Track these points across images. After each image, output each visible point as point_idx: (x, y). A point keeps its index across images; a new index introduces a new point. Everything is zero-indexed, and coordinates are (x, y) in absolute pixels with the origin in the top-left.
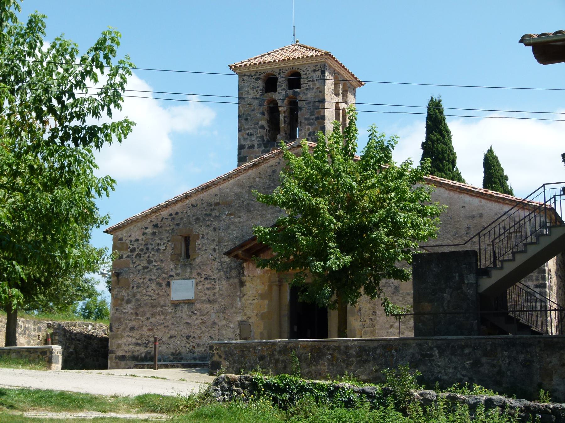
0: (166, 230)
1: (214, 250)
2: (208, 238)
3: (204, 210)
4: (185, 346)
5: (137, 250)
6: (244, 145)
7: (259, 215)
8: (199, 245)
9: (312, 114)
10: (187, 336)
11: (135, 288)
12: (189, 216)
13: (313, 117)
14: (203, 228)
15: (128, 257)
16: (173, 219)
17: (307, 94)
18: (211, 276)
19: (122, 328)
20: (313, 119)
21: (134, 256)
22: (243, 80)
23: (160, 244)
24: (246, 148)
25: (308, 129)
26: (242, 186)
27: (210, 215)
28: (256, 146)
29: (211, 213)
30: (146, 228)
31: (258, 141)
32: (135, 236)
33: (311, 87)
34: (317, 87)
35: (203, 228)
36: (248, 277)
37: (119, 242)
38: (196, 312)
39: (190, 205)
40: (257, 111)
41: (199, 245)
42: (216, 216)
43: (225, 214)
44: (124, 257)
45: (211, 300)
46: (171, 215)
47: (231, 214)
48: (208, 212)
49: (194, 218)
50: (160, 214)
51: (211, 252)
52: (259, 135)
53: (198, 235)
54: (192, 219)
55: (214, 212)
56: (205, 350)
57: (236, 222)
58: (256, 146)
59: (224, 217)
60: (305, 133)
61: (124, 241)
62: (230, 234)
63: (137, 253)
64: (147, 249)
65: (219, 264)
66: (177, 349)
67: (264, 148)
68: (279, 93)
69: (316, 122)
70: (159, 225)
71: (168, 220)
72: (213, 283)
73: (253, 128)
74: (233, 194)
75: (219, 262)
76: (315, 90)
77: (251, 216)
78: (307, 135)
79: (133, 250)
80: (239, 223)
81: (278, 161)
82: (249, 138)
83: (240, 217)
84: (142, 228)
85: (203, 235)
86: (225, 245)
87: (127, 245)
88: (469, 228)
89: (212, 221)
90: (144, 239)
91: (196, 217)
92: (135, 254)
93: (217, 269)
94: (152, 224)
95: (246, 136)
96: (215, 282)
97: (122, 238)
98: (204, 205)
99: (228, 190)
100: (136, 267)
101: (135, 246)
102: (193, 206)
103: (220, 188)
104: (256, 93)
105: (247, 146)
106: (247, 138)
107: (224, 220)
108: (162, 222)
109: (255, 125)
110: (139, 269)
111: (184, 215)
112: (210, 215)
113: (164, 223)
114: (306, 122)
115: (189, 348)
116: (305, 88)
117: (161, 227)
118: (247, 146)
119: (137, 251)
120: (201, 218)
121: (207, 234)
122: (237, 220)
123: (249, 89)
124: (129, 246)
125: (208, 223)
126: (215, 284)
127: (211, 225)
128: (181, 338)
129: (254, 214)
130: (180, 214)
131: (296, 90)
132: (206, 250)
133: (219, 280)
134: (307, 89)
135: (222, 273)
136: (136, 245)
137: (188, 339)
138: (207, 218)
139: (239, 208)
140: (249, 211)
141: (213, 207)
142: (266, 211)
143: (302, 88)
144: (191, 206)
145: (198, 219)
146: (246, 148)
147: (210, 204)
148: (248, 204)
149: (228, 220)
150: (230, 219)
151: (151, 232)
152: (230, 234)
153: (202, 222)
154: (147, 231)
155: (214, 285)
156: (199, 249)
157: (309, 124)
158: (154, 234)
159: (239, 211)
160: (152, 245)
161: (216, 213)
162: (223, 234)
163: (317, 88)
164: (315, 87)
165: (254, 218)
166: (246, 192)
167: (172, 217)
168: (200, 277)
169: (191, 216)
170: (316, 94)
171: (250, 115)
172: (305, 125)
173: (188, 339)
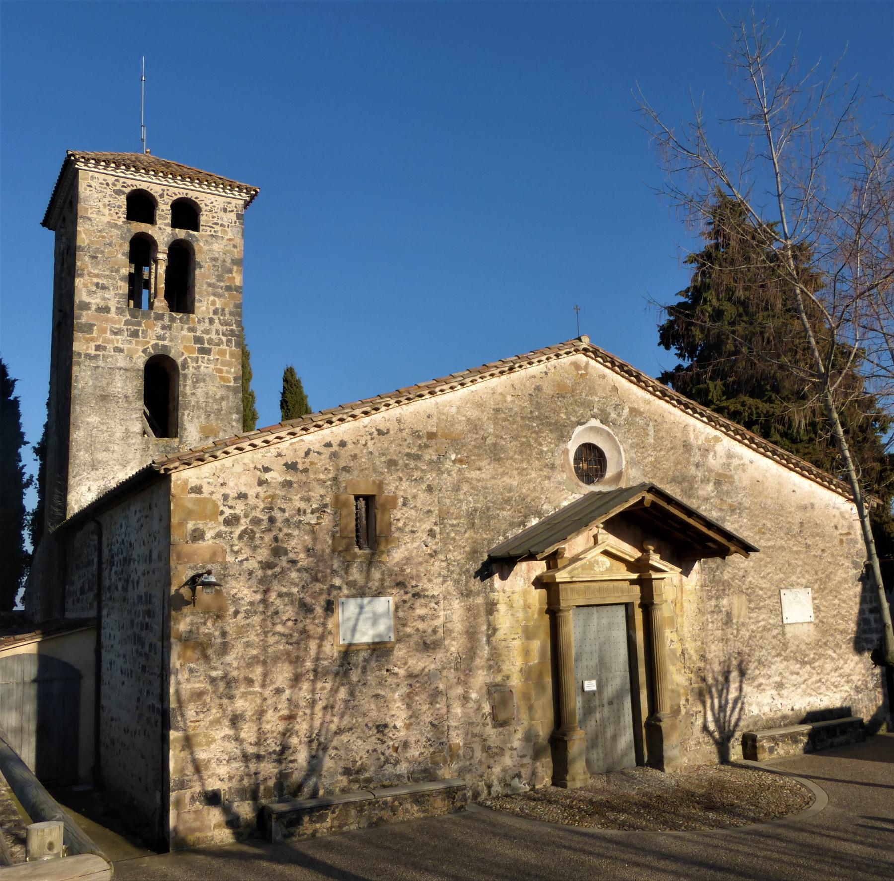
0: (319, 480)
1: (431, 533)
2: (415, 507)
3: (406, 443)
4: (375, 750)
5: (243, 521)
6: (90, 303)
7: (517, 469)
8: (398, 520)
9: (220, 278)
10: (378, 727)
11: (240, 616)
12: (371, 453)
13: (222, 284)
14: (405, 485)
15: (219, 535)
16: (334, 455)
17: (211, 243)
18: (426, 590)
19: (208, 719)
20: (221, 288)
21: (236, 535)
22: (90, 186)
23: (305, 512)
24: (93, 309)
25: (213, 303)
26: (480, 406)
27: (418, 457)
28: (113, 309)
29: (420, 453)
30: (266, 469)
31: (118, 302)
32: (236, 485)
33: (219, 234)
34: (229, 237)
35: (405, 485)
36: (501, 594)
37: (193, 495)
38: (396, 670)
39: (374, 430)
40: (118, 248)
41: (398, 520)
42: (431, 462)
43: (450, 459)
44: (208, 535)
45: (428, 642)
46: (328, 445)
47: (461, 461)
48: (414, 450)
49: (383, 459)
50: (302, 440)
51: (424, 538)
52: (121, 292)
53: (395, 498)
54: (380, 462)
55: (426, 451)
56: (422, 754)
57: (472, 478)
58: (113, 309)
59: (448, 464)
60: (207, 308)
61: (205, 495)
62: (461, 501)
63: (243, 528)
64: (272, 520)
65: (444, 564)
66: (357, 759)
67: (129, 317)
68: (160, 228)
69: (227, 294)
70: (300, 467)
71: (323, 456)
72: (433, 605)
73: (107, 277)
74: (464, 419)
75: (443, 561)
76: (225, 242)
77: (500, 470)
78: (211, 311)
79: (232, 521)
80: (479, 480)
81: (545, 369)
82: (100, 293)
83: (480, 469)
84: (255, 468)
85: (405, 499)
86: (453, 525)
87: (216, 506)
88: (801, 524)
89: (422, 470)
90: (262, 495)
91: (389, 457)
92: (238, 531)
93: (439, 574)
94: (282, 461)
95: (94, 288)
96: (436, 603)
97: (201, 487)
98: (404, 434)
99: (454, 410)
100: (241, 562)
101: (238, 511)
102: (380, 433)
103: (437, 404)
104: (115, 217)
105: (94, 307)
106: (95, 292)
107: (449, 472)
108: (307, 460)
109: (112, 272)
110: (251, 568)
111: (361, 451)
112: (418, 457)
113: (312, 463)
114: (210, 289)
115: (383, 754)
116: (208, 233)
117: (306, 470)
118: (94, 307)
119: (244, 524)
120: (401, 462)
121: (414, 497)
122: (475, 474)
123: (101, 204)
124: (222, 508)
125: (417, 474)
126: (436, 607)
127: (421, 478)
128: (364, 732)
129: (507, 465)
130: (350, 446)
131: (191, 232)
132: (413, 532)
133: (445, 598)
134: (212, 235)
135: (450, 583)
136: (240, 508)
137: (382, 732)
138: (412, 464)
139: (476, 451)
140: (498, 460)
141: (425, 440)
142: (529, 462)
143: (201, 232)
144: (376, 433)
145: (392, 463)
146: (93, 309)
147: (416, 434)
148: (495, 445)
149: (457, 473)
150: (460, 470)
151: (280, 479)
152: (461, 501)
153: (403, 470)
154: (268, 476)
155: (435, 610)
156: (399, 529)
157: (214, 295)
158: (287, 484)
159: (479, 455)
160: (283, 511)
161: (431, 455)
162: (448, 501)
163: (230, 240)
164: (226, 237)
165: (507, 473)
166: (488, 419)
167: (332, 449)
168: (402, 592)
169: (376, 453)
170: (227, 248)
171: (102, 253)
172: (208, 294)
173: (382, 732)
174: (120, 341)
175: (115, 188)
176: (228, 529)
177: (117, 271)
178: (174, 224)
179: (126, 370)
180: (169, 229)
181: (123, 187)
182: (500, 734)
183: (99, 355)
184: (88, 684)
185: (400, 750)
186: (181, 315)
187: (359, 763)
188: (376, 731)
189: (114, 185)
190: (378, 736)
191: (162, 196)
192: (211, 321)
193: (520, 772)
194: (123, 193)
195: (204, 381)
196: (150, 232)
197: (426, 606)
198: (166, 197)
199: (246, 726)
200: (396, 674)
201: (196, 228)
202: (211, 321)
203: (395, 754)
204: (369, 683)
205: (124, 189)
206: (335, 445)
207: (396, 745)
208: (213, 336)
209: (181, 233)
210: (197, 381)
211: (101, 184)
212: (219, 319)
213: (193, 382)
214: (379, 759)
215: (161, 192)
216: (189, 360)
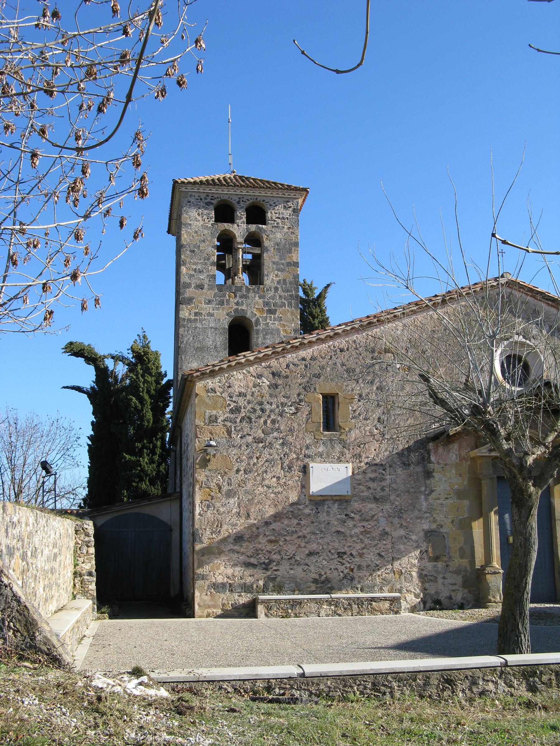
20: (283, 264)
22: (190, 202)
45: (378, 497)
64: (263, 410)
67: (216, 291)
72: (381, 471)
96: (384, 470)
114: (275, 266)
115: (342, 572)
126: (384, 472)
131: (260, 226)
133: (390, 466)
137: (342, 557)
155: (383, 475)
157: (278, 270)
173: (342, 557)
174: (209, 308)
175: (206, 201)
176: (232, 416)
177: (208, 259)
178: (249, 222)
179: (216, 329)
180: (245, 226)
181: (212, 199)
182: (435, 566)
183: (197, 319)
184: (176, 535)
185: (355, 570)
186: (254, 286)
187: (325, 576)
188: (337, 556)
189: (205, 199)
190: (339, 559)
191: (239, 202)
192: (276, 289)
193: (451, 595)
194: (212, 204)
195: (272, 334)
196: (231, 229)
197: (376, 471)
198: (241, 202)
199: (245, 545)
200: (353, 518)
201: (264, 223)
202: (276, 289)
203: (351, 573)
204: (331, 523)
205: (212, 201)
206: (308, 359)
207: (352, 567)
208: (278, 300)
209: (253, 227)
210: (266, 334)
211: (197, 199)
212: (282, 288)
213: (263, 334)
214: (340, 575)
215: (238, 200)
216: (260, 319)
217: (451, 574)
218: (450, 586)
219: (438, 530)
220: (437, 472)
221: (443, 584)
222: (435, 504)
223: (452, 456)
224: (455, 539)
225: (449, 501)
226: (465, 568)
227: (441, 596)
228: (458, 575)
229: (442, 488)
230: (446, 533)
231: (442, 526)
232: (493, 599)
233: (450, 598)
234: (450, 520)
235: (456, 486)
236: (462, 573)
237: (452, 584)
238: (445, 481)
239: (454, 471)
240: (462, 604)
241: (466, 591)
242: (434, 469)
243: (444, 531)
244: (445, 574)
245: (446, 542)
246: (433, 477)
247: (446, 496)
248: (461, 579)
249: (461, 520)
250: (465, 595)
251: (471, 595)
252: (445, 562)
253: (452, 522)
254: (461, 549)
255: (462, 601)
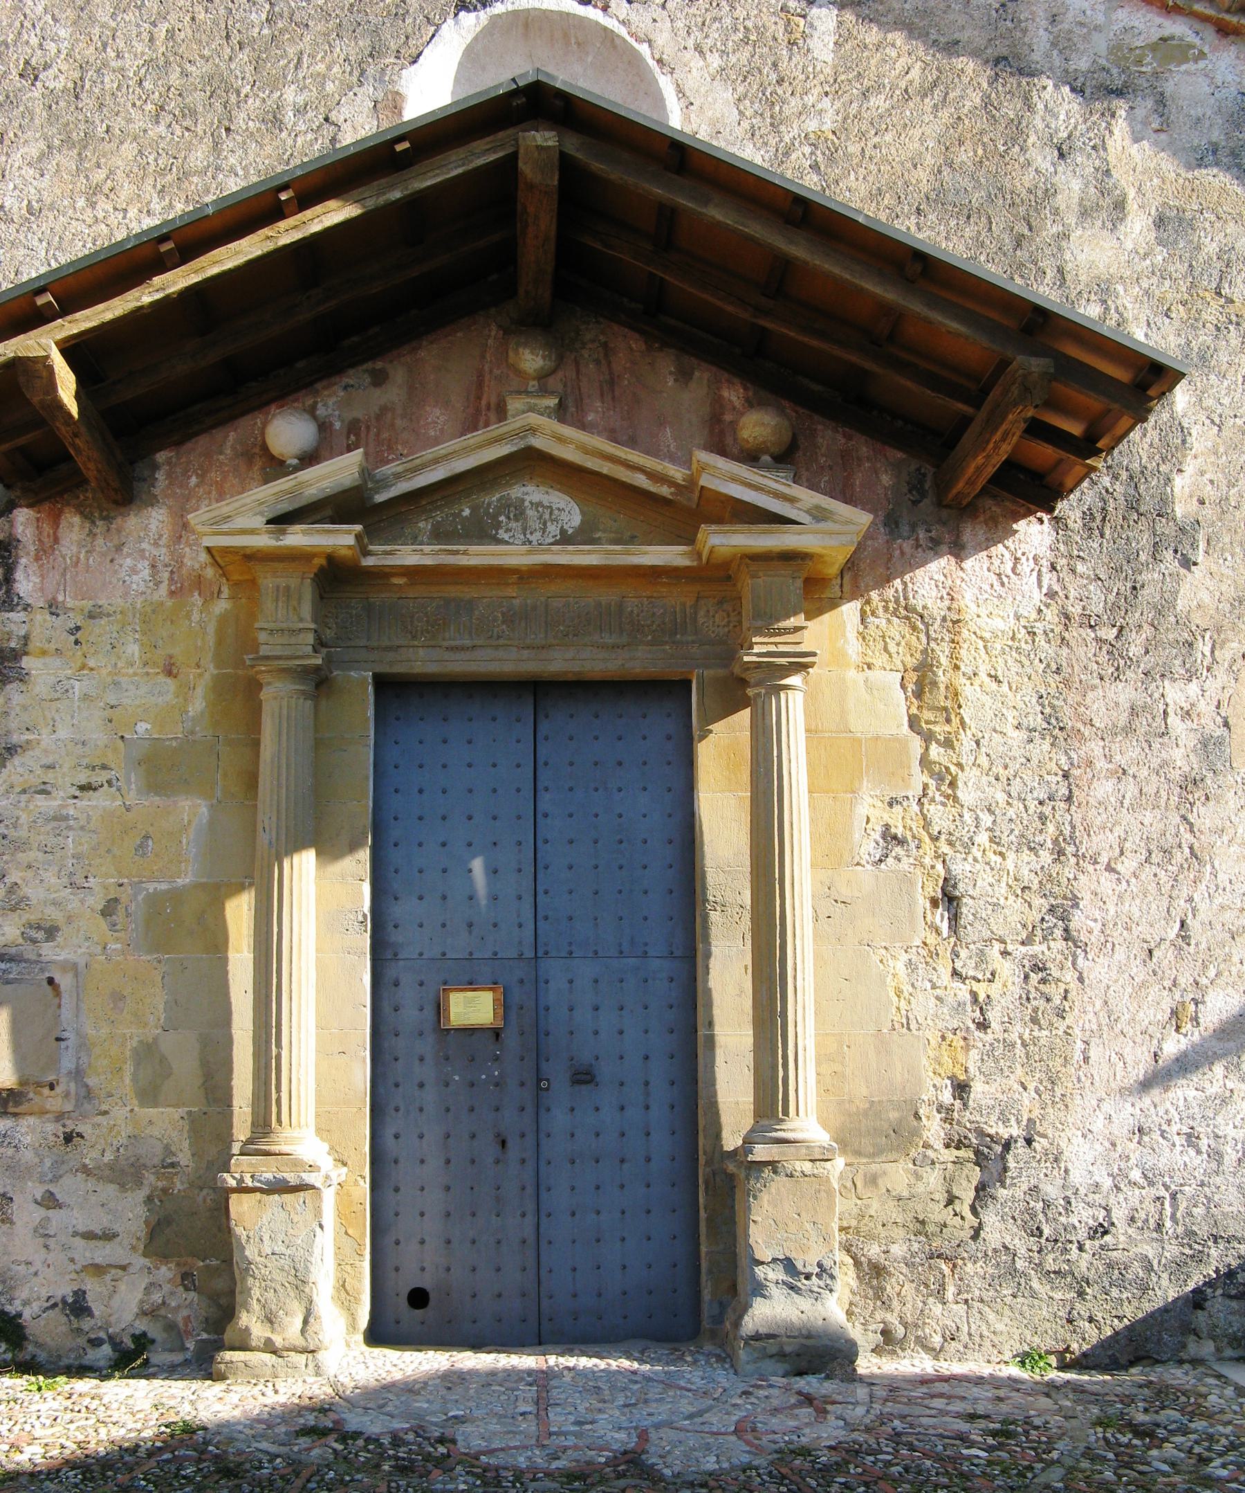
193: (80, 1295)
217: (91, 1184)
218: (78, 1241)
219: (29, 952)
220: (44, 653)
221: (42, 1233)
222: (24, 818)
223: (134, 571)
224: (118, 998)
225: (101, 801)
226: (168, 1150)
227: (23, 1293)
228: (122, 1186)
229: (63, 733)
230: (73, 968)
231: (51, 932)
232: (258, 1331)
233: (78, 1307)
234: (97, 901)
235: (142, 727)
236: (150, 1178)
237: (89, 1236)
238: (86, 697)
239: (133, 650)
240: (143, 1342)
241: (166, 1272)
242: (26, 638)
243: (63, 956)
244: (56, 1179)
245: (67, 1013)
246: (23, 678)
247: (83, 778)
248: (142, 1211)
249: (155, 901)
250: (157, 1297)
251: (192, 1295)
252: (60, 1117)
253: (108, 910)
254: (147, 1052)
255: (141, 1326)
